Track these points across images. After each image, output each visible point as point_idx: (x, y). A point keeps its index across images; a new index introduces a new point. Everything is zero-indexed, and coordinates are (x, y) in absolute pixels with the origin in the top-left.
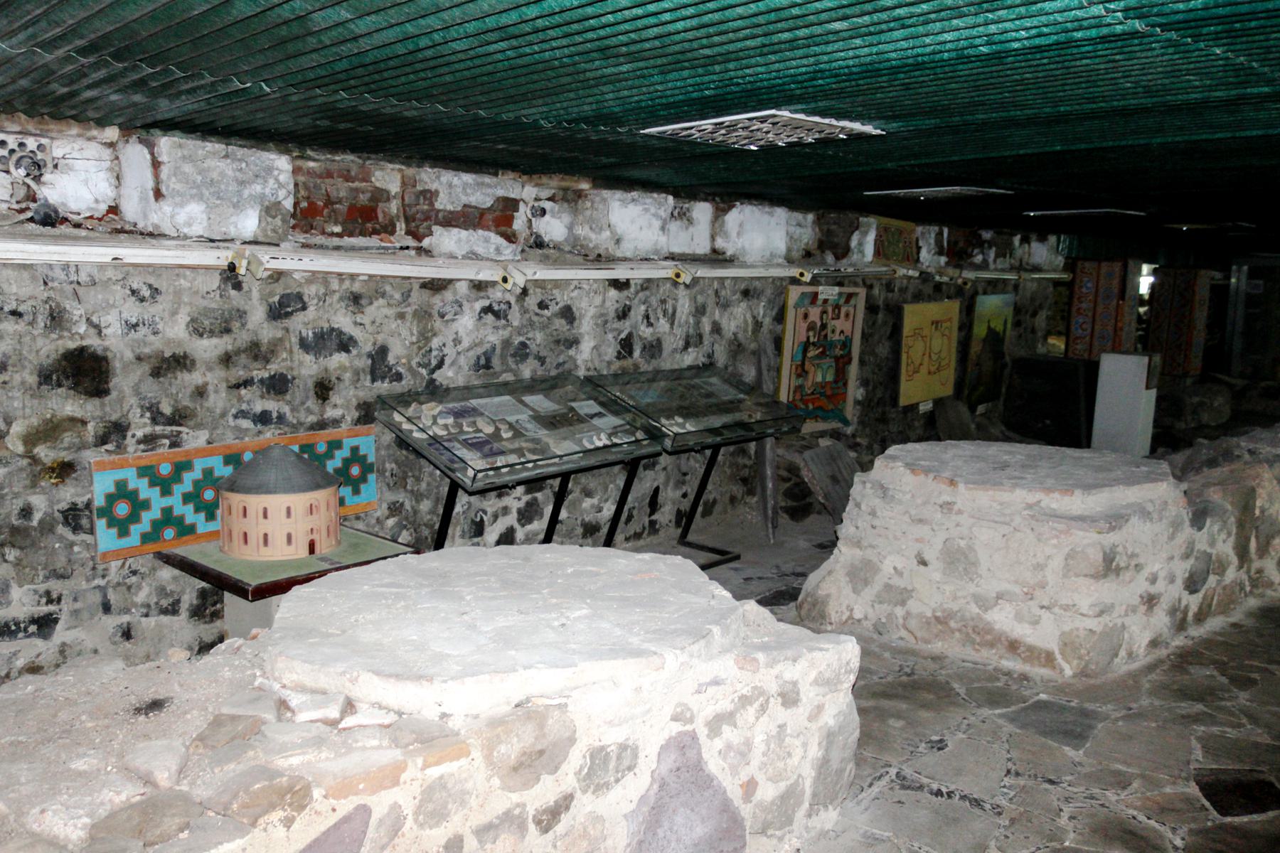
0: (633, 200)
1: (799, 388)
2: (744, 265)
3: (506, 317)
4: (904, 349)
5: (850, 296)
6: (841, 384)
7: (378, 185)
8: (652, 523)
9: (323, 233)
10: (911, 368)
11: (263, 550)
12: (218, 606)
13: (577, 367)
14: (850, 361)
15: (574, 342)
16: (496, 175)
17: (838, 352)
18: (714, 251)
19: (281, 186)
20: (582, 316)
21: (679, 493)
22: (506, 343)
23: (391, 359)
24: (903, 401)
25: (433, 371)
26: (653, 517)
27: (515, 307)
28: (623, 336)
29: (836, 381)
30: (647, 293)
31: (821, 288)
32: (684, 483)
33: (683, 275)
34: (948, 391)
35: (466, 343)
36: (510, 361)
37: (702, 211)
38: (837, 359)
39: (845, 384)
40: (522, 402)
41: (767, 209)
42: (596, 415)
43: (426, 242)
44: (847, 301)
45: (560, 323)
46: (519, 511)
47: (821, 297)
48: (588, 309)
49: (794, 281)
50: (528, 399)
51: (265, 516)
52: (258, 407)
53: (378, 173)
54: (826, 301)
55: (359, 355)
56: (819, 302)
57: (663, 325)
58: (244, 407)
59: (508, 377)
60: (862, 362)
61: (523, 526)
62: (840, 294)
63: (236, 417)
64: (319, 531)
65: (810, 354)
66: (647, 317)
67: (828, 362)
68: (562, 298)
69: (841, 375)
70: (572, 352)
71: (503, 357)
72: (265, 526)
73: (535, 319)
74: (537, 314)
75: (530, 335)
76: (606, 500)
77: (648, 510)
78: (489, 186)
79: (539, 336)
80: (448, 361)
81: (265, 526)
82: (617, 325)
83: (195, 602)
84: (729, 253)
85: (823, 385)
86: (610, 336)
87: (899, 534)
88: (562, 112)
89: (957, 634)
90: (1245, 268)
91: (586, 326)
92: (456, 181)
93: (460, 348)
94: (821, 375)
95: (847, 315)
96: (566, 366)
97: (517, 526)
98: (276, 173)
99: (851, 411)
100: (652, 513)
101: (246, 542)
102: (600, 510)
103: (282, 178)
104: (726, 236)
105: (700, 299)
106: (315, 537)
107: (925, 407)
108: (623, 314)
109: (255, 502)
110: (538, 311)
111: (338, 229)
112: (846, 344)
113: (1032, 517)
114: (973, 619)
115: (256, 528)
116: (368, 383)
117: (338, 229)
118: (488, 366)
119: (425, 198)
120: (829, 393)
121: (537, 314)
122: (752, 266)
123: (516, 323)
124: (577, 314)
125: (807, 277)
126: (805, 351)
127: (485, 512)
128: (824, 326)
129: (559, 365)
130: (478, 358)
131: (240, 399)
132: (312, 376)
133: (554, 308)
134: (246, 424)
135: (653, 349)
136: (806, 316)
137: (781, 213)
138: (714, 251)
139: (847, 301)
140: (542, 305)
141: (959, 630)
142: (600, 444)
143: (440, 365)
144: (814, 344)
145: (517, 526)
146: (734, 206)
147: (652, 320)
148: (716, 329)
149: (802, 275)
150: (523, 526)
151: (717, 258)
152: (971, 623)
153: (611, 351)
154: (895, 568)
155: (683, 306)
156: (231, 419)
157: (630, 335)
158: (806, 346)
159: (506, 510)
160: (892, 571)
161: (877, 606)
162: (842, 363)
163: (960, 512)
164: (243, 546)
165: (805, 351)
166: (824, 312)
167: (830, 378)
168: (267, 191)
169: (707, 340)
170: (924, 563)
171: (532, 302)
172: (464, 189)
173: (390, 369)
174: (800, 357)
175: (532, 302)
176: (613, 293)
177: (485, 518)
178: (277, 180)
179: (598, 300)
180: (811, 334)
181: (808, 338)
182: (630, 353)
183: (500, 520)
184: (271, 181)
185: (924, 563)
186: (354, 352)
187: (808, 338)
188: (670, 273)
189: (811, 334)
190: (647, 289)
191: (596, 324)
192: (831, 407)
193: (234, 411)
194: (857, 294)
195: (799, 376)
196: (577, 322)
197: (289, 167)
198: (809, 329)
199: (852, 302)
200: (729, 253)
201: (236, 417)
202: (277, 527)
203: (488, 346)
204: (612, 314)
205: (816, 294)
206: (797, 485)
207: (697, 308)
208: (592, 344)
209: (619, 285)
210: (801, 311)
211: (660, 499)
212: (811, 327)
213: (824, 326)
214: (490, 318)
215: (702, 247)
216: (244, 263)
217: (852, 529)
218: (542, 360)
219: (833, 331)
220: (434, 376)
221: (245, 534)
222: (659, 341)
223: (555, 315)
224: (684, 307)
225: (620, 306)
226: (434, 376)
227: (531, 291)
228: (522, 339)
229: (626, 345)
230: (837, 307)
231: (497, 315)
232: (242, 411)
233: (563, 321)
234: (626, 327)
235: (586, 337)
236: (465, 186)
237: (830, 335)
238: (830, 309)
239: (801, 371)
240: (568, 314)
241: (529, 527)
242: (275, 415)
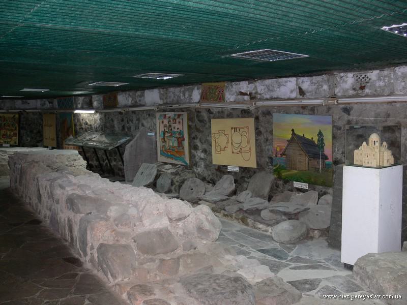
1: (164, 146)
2: (146, 106)
14: (184, 140)
45: (111, 122)
54: (169, 117)
56: (167, 118)
65: (166, 135)
136: (163, 122)
158: (164, 132)
165: (164, 134)
166: (169, 121)
171: (107, 117)
176: (120, 115)
180: (165, 128)
181: (165, 130)
187: (165, 130)
195: (163, 142)
198: (164, 127)
205: (165, 115)
210: (161, 121)
212: (165, 126)
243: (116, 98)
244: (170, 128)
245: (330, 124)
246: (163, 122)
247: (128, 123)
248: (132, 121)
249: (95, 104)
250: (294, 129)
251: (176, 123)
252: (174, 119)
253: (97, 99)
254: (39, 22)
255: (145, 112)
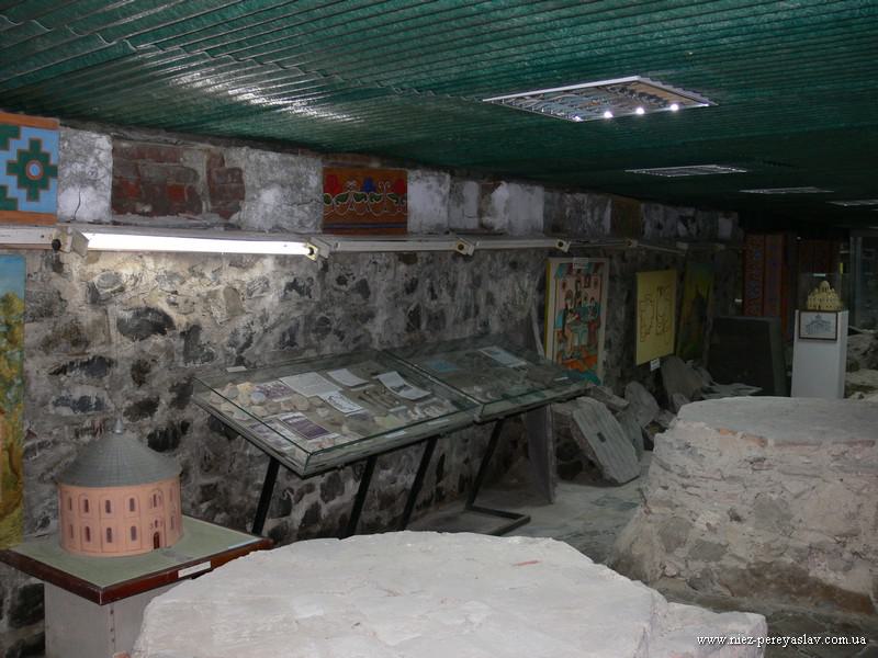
0: (418, 178)
1: (561, 352)
2: (513, 238)
3: (309, 293)
4: (638, 313)
5: (597, 266)
6: (592, 347)
7: (186, 164)
8: (439, 490)
9: (134, 212)
10: (643, 331)
11: (107, 546)
12: (41, 605)
13: (371, 340)
14: (599, 327)
15: (370, 316)
16: (296, 154)
17: (590, 317)
18: (482, 226)
19: (101, 165)
20: (376, 290)
21: (462, 459)
22: (309, 318)
23: (203, 338)
24: (640, 360)
25: (242, 350)
26: (440, 485)
27: (317, 284)
28: (412, 308)
29: (589, 345)
30: (432, 267)
31: (575, 259)
32: (465, 449)
33: (465, 246)
34: (670, 349)
35: (272, 320)
36: (312, 337)
37: (471, 189)
38: (590, 324)
39: (596, 347)
40: (329, 378)
41: (528, 187)
42: (401, 388)
43: (234, 218)
44: (595, 271)
45: (357, 298)
46: (322, 487)
47: (575, 267)
48: (382, 285)
49: (553, 253)
50: (336, 374)
51: (108, 511)
52: (77, 394)
53: (186, 154)
54: (579, 271)
55: (173, 336)
56: (574, 273)
57: (445, 297)
58: (64, 393)
59: (311, 354)
60: (607, 329)
61: (326, 502)
62: (590, 264)
63: (56, 404)
64: (163, 523)
65: (568, 321)
66: (432, 290)
67: (583, 327)
68: (361, 272)
69: (592, 335)
70: (368, 326)
71: (305, 333)
72: (108, 521)
73: (335, 294)
74: (336, 290)
75: (329, 311)
76: (400, 471)
77: (435, 478)
78: (292, 163)
79: (339, 312)
80: (255, 340)
81: (108, 521)
82: (407, 298)
83: (17, 603)
84: (496, 228)
85: (579, 349)
86: (400, 309)
87: (711, 492)
88: (424, 76)
89: (773, 586)
90: (860, 239)
91: (380, 300)
92: (263, 158)
93: (267, 325)
94: (578, 339)
95: (596, 284)
96: (362, 341)
97: (321, 502)
98: (96, 151)
99: (600, 373)
100: (439, 481)
101: (88, 538)
102: (394, 481)
103: (102, 156)
104: (494, 213)
105: (477, 272)
106: (160, 529)
107: (654, 366)
108: (411, 288)
109: (97, 495)
110: (336, 286)
111: (147, 209)
112: (596, 310)
113: (841, 468)
114: (788, 570)
115: (98, 526)
116: (181, 364)
117: (147, 209)
118: (292, 343)
119: (233, 176)
120: (584, 356)
121: (336, 290)
122: (520, 238)
123: (317, 299)
124: (372, 289)
125: (565, 248)
126: (565, 318)
127: (292, 491)
128: (578, 294)
129: (357, 339)
130: (284, 335)
131: (61, 386)
132: (128, 359)
133: (352, 283)
134: (66, 411)
135: (437, 320)
136: (564, 285)
137: (539, 191)
138: (482, 226)
139: (595, 271)
140: (341, 281)
141: (775, 582)
142: (415, 418)
143: (247, 345)
144: (571, 311)
145: (321, 502)
146: (499, 185)
147: (436, 292)
148: (490, 299)
149: (561, 244)
150: (326, 502)
151: (486, 231)
152: (787, 573)
153: (401, 321)
154: (708, 525)
155: (462, 278)
156: (50, 406)
157: (418, 308)
158: (566, 312)
159: (310, 489)
160: (705, 528)
161: (690, 563)
162: (593, 327)
163: (770, 466)
164: (85, 543)
165: (565, 318)
166: (578, 281)
167: (584, 342)
168: (87, 170)
169: (482, 311)
170: (737, 519)
171: (332, 276)
172: (271, 167)
173: (202, 350)
174: (561, 324)
175: (332, 276)
176: (402, 267)
177: (292, 497)
178: (97, 159)
179: (390, 274)
180: (569, 301)
181: (567, 306)
182: (419, 326)
183: (306, 496)
184: (92, 160)
185: (737, 519)
186: (169, 333)
187: (567, 306)
188: (453, 246)
189: (569, 301)
190: (431, 262)
191: (389, 298)
192: (586, 368)
193: (54, 398)
194: (602, 264)
195: (560, 342)
196: (372, 296)
197: (109, 146)
198: (567, 298)
199: (599, 272)
200: (496, 228)
201: (56, 404)
202: (121, 521)
203: (292, 323)
204: (401, 288)
205: (571, 266)
206: (566, 445)
207: (473, 280)
208: (385, 317)
209: (408, 258)
210: (560, 281)
211: (446, 467)
212: (568, 296)
213: (578, 294)
214: (294, 293)
215: (473, 224)
216: (69, 240)
217: (660, 491)
218: (341, 335)
219: (586, 299)
220: (243, 354)
221: (88, 530)
222: (442, 312)
223: (352, 290)
224: (464, 279)
225: (408, 280)
226: (243, 354)
227: (331, 267)
228: (322, 314)
229: (414, 318)
230: (588, 276)
231: (300, 291)
232: (62, 398)
233: (359, 295)
234: (414, 299)
235: (380, 311)
236: (272, 163)
237: (583, 302)
238: (583, 278)
239: (562, 337)
240: (363, 288)
241: (332, 503)
242: (94, 401)
243: (401, 189)
244: (578, 301)
245: (258, 489)
246: (564, 285)
247: (434, 297)
248: (452, 287)
249: (158, 189)
250: (138, 528)
251: (589, 286)
252: (588, 276)
253: (281, 174)
254: (633, 69)
255: (498, 255)
